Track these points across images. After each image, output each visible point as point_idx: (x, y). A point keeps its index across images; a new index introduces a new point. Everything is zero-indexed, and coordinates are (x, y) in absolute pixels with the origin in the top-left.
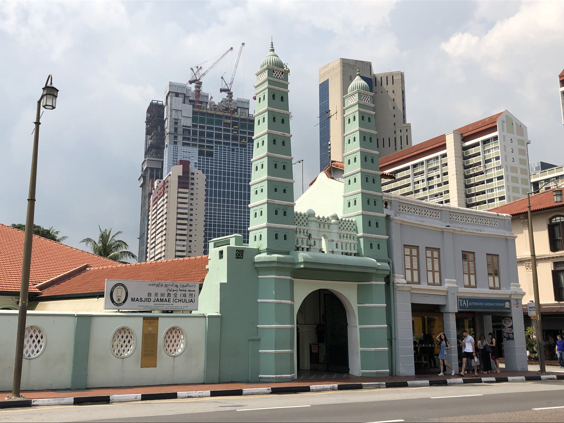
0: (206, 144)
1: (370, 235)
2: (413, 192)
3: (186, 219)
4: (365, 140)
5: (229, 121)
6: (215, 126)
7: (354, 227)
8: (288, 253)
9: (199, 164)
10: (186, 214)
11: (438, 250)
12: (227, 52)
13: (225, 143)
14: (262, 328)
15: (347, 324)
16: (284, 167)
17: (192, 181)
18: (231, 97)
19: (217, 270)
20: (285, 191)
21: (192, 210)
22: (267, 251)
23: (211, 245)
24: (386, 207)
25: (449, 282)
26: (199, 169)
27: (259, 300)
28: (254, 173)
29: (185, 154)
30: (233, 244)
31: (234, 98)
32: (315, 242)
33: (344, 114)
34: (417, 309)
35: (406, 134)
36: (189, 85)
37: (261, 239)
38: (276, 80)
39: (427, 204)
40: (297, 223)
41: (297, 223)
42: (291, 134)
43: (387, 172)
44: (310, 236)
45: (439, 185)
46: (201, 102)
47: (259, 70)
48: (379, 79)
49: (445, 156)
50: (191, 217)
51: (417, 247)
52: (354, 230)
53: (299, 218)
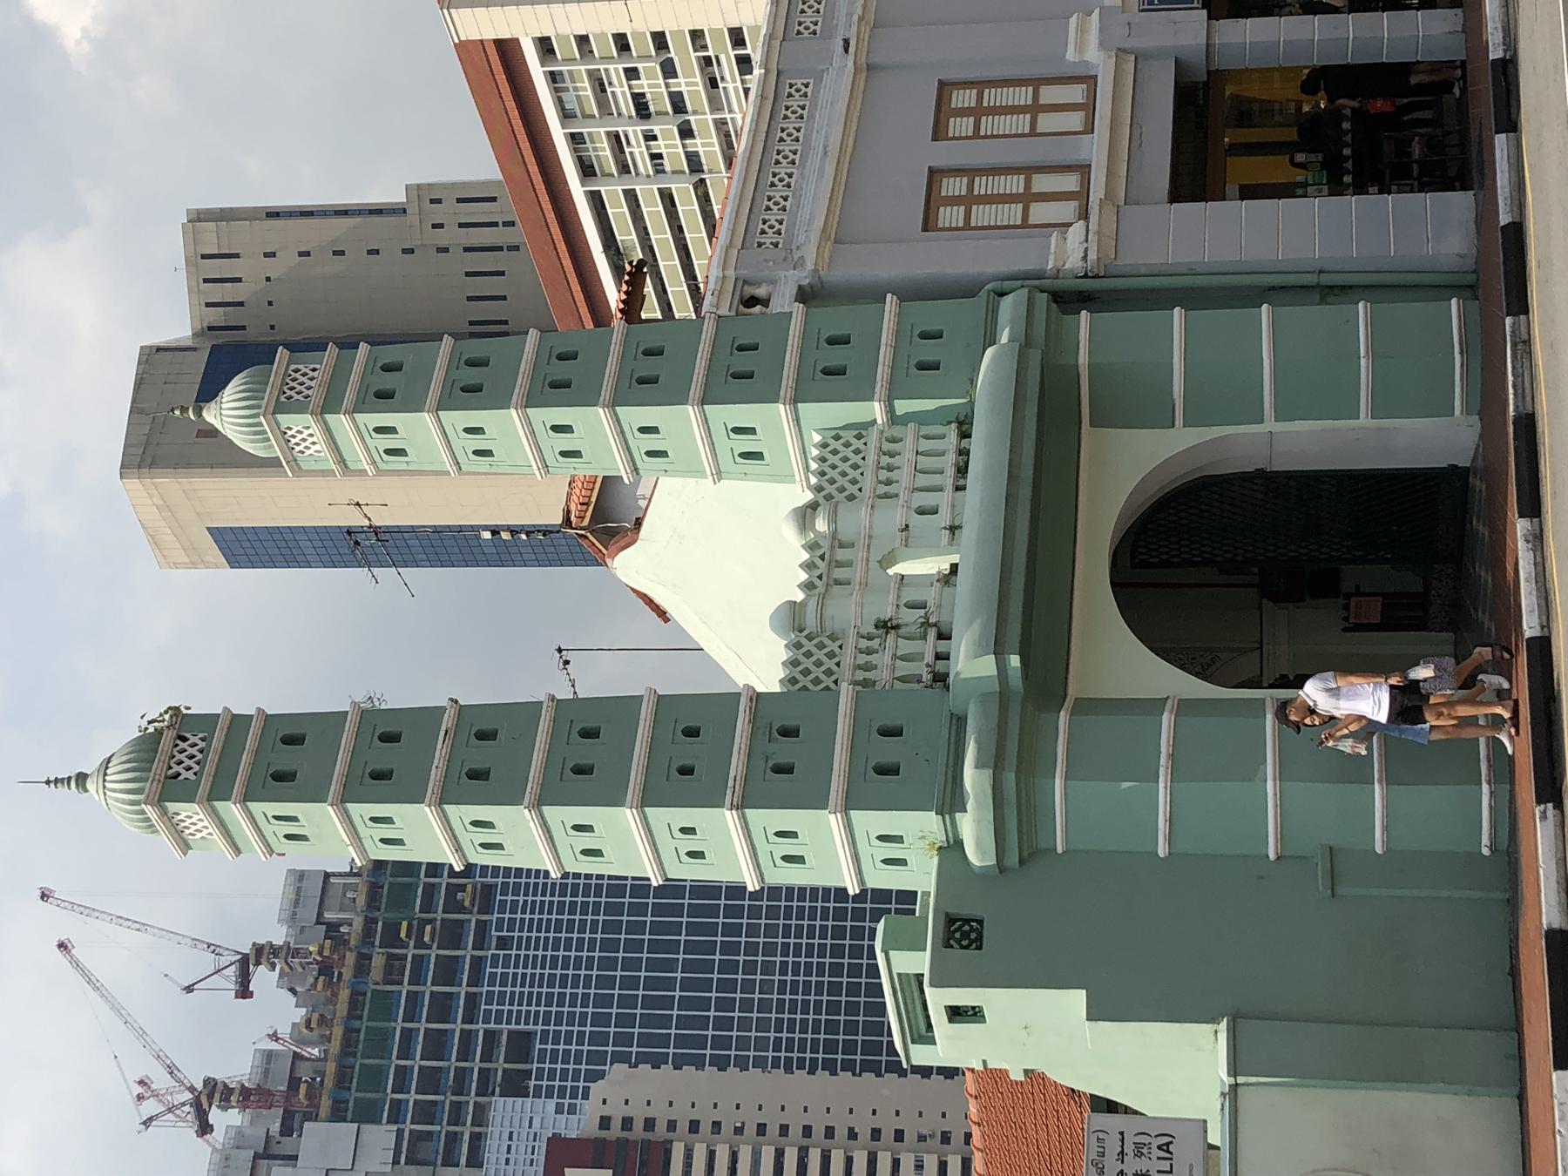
0: (477, 1065)
1: (882, 372)
2: (696, 177)
3: (803, 1153)
4: (477, 389)
5: (378, 961)
6: (399, 1025)
7: (848, 435)
8: (959, 722)
9: (562, 1095)
10: (780, 1154)
11: (944, 88)
12: (77, 965)
13: (475, 980)
14: (1282, 838)
15: (1260, 473)
16: (589, 734)
17: (638, 1125)
18: (275, 951)
19: (1035, 1032)
20: (691, 732)
21: (761, 1129)
22: (952, 812)
23: (921, 1055)
24: (765, 302)
25: (1081, 46)
26: (586, 1097)
27: (1162, 850)
28: (611, 866)
29: (519, 1155)
30: (918, 962)
31: (278, 935)
32: (911, 606)
33: (363, 472)
34: (1193, 179)
35: (449, 205)
36: (218, 1135)
37: (898, 839)
38: (210, 768)
39: (755, 132)
40: (828, 682)
41: (828, 682)
42: (444, 703)
43: (613, 295)
44: (887, 626)
45: (669, 70)
46: (294, 1083)
47: (164, 839)
48: (216, 316)
49: (545, 46)
50: (795, 1131)
51: (934, 175)
52: (859, 437)
53: (806, 672)
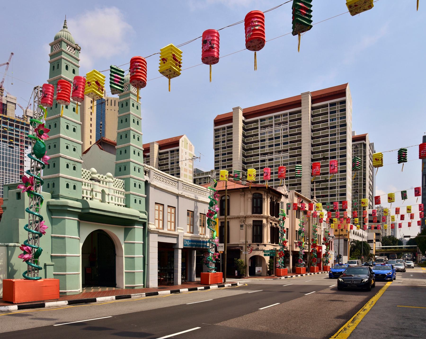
51: (163, 205)
